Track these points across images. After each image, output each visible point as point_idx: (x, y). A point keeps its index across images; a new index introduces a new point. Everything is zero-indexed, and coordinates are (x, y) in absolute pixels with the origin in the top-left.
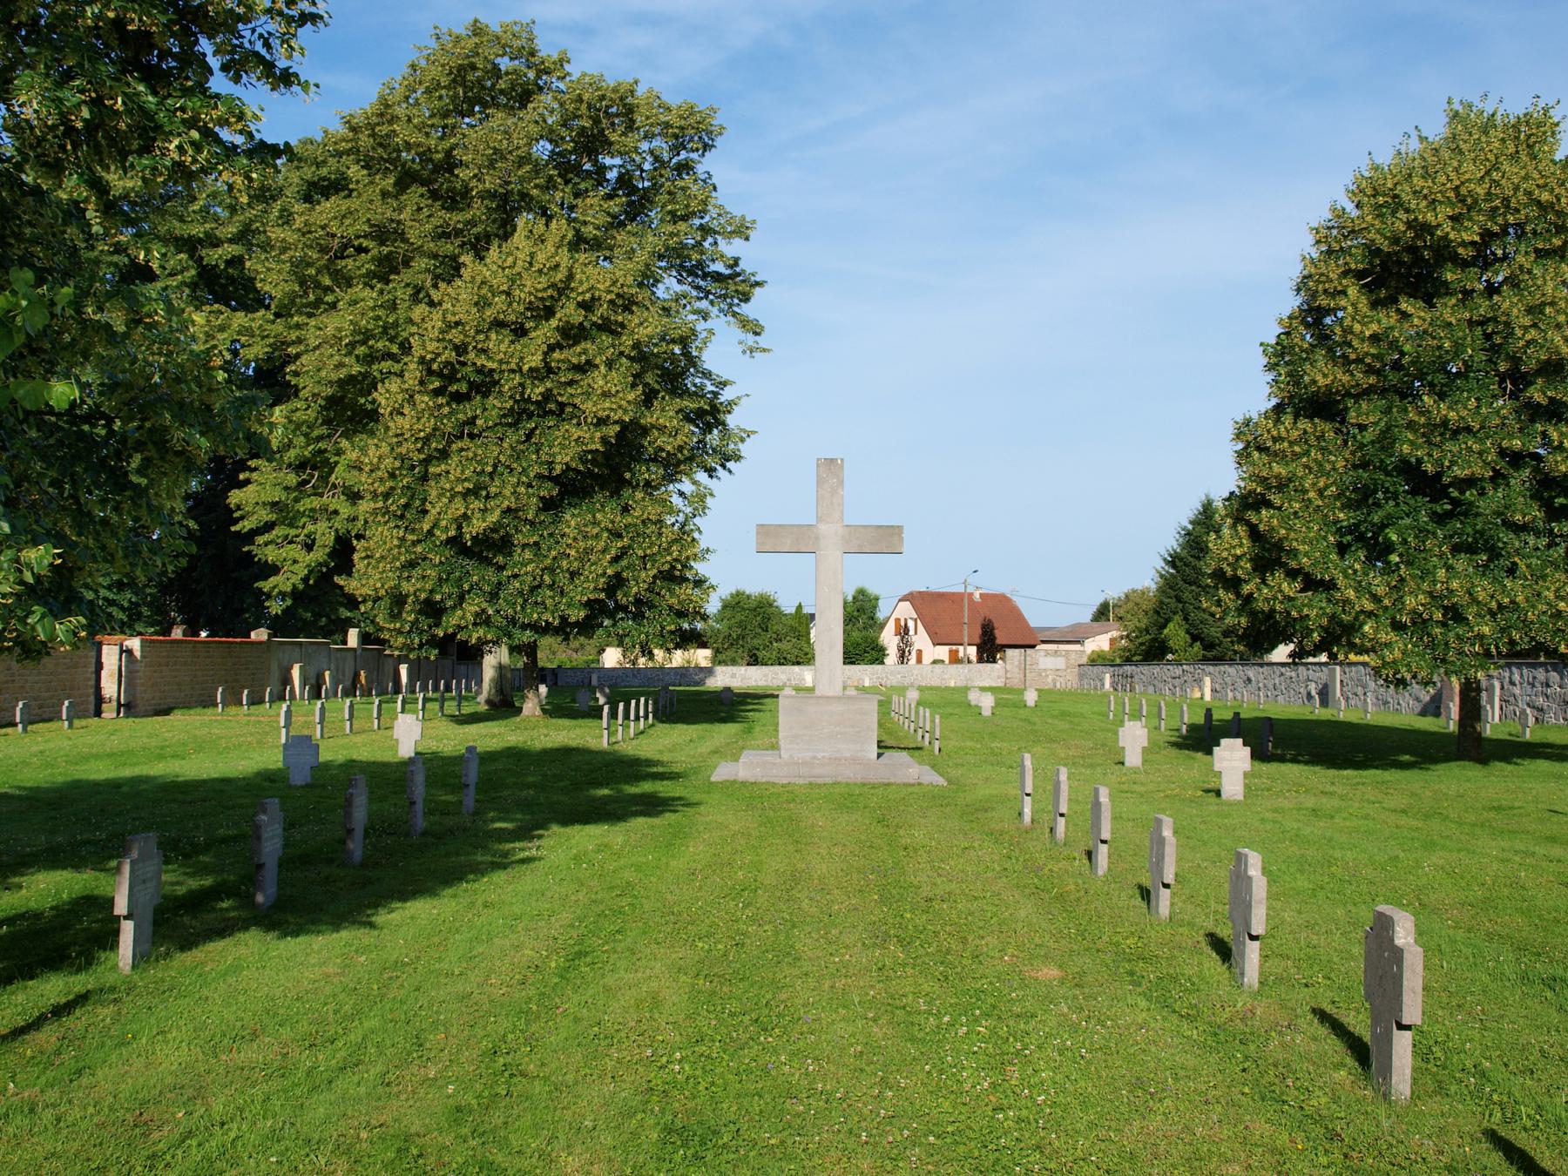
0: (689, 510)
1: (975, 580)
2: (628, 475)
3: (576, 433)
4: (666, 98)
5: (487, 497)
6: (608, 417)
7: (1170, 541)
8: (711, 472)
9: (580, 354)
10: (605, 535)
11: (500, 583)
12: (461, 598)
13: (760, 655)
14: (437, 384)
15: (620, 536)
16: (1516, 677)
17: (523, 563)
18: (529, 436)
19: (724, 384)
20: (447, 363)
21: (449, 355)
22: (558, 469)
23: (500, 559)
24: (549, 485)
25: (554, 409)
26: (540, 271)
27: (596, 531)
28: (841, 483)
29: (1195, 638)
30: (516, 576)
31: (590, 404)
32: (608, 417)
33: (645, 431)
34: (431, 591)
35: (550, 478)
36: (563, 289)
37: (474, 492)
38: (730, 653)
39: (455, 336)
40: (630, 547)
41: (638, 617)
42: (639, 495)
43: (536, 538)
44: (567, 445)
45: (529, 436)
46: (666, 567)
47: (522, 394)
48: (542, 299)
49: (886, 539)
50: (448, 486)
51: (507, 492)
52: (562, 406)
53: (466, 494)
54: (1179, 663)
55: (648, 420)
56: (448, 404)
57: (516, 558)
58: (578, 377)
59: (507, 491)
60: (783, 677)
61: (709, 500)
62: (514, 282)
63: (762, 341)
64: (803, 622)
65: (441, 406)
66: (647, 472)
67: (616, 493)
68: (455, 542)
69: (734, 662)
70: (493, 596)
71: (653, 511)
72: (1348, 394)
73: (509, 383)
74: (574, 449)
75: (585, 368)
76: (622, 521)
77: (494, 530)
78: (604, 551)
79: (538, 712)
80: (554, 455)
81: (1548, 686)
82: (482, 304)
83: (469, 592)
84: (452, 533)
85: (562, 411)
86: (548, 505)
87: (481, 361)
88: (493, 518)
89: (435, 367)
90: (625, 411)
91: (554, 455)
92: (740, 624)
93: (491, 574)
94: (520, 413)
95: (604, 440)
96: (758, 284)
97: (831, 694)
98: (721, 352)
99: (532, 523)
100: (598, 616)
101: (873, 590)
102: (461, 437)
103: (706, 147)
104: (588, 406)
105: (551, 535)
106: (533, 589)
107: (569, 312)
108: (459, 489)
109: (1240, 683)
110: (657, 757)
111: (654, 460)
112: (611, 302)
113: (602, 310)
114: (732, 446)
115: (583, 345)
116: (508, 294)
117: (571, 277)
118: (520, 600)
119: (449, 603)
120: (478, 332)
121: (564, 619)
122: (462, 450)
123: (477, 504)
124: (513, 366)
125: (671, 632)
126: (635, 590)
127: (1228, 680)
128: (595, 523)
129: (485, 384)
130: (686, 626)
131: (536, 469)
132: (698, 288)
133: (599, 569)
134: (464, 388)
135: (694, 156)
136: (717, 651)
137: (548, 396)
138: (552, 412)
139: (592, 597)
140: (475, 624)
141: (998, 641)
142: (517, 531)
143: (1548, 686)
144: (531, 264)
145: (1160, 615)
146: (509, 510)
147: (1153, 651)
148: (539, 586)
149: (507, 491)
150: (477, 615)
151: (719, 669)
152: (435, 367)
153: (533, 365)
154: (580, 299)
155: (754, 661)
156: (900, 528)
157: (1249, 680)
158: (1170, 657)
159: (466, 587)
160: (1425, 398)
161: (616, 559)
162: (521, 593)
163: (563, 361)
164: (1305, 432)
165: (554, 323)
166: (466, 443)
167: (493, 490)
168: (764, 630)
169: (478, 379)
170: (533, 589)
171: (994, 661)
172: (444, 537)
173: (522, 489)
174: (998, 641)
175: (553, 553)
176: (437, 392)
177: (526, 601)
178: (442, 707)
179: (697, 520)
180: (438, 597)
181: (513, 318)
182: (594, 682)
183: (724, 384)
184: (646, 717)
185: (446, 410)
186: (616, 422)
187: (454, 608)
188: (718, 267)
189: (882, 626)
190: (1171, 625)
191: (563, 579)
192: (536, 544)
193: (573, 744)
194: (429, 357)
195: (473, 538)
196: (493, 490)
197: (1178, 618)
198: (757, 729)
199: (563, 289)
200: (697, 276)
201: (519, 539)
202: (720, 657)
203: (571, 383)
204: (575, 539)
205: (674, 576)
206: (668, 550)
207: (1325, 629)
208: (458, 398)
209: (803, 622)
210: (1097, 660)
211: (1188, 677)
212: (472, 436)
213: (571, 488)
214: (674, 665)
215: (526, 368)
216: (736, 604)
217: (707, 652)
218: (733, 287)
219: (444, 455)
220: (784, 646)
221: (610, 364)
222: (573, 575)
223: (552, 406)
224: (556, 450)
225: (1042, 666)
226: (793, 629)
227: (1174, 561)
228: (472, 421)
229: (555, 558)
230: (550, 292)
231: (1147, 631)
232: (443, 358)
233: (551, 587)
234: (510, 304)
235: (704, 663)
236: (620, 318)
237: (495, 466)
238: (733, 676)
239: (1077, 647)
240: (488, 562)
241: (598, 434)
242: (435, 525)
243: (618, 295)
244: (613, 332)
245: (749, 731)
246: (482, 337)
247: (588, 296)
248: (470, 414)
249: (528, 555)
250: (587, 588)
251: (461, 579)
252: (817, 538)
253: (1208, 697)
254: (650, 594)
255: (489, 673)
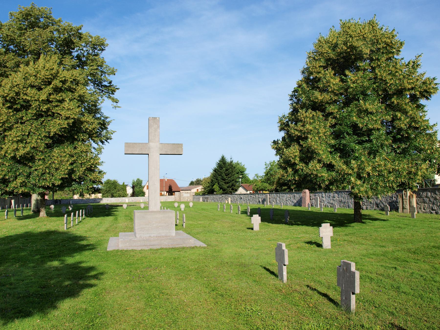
0: (96, 153)
1: (166, 176)
2: (76, 137)
3: (58, 122)
4: (91, 34)
5: (26, 143)
6: (69, 117)
7: (214, 166)
8: (102, 142)
9: (60, 97)
10: (68, 155)
11: (30, 172)
12: (16, 178)
13: (114, 195)
14: (9, 105)
15: (73, 156)
16: (324, 195)
17: (39, 166)
18: (42, 123)
19: (107, 118)
20: (12, 98)
21: (12, 94)
22: (52, 134)
23: (30, 164)
24: (49, 139)
25: (49, 114)
26: (47, 70)
27: (65, 154)
28: (159, 127)
29: (221, 188)
30: (36, 170)
31: (63, 112)
32: (69, 117)
33: (82, 123)
34: (5, 175)
35: (49, 137)
36: (55, 76)
37: (21, 141)
38: (106, 195)
39: (16, 89)
40: (76, 160)
41: (80, 183)
42: (80, 143)
43: (43, 157)
44: (55, 126)
45: (42, 123)
46: (89, 166)
47: (39, 108)
48: (47, 78)
49: (175, 150)
50: (11, 139)
51: (33, 141)
52: (53, 113)
53: (18, 142)
54: (217, 194)
55: (83, 119)
56: (13, 112)
57: (36, 164)
58: (59, 104)
59: (33, 141)
60: (121, 200)
61: (102, 150)
62: (38, 73)
63: (119, 104)
64: (124, 187)
65: (10, 112)
66: (81, 136)
67: (72, 143)
68: (14, 158)
69: (107, 197)
70: (28, 177)
71: (84, 148)
72: (327, 103)
73: (34, 105)
74: (58, 127)
75: (62, 101)
76: (74, 152)
77: (28, 154)
78: (68, 161)
79: (45, 215)
80: (50, 129)
81: (334, 197)
82: (26, 79)
83: (19, 175)
84: (12, 155)
85: (54, 115)
86: (48, 146)
87: (25, 97)
88: (28, 149)
89: (8, 98)
90: (76, 115)
91: (50, 129)
92: (109, 187)
93: (27, 169)
94: (39, 115)
95: (68, 124)
96: (117, 89)
97: (155, 210)
98: (106, 106)
99: (42, 152)
100: (67, 182)
101: (141, 179)
102: (18, 123)
103: (102, 50)
104: (63, 113)
105: (49, 156)
106: (43, 174)
107: (56, 83)
108: (15, 139)
109: (239, 199)
110: (84, 234)
111: (85, 132)
112: (71, 82)
113: (68, 84)
114: (109, 135)
115: (61, 93)
116: (36, 76)
117: (58, 72)
118: (38, 178)
119: (11, 179)
120: (24, 87)
121: (53, 184)
122: (17, 127)
123: (21, 145)
124: (36, 98)
125: (91, 188)
126: (78, 174)
127: (235, 198)
128: (65, 152)
129: (27, 106)
130: (95, 186)
131: (44, 134)
132: (100, 89)
133: (66, 167)
134: (19, 106)
135: (99, 52)
136: (103, 194)
137: (48, 109)
138: (50, 115)
139: (63, 176)
140: (21, 186)
141: (173, 190)
142: (37, 155)
143: (334, 197)
144: (44, 68)
145: (212, 183)
146: (34, 147)
147: (211, 192)
148: (45, 173)
149: (33, 141)
150: (21, 183)
151: (104, 199)
152: (8, 98)
153: (43, 98)
154: (61, 79)
155: (113, 196)
156: (182, 144)
157: (241, 198)
158: (215, 193)
159: (18, 174)
160: (361, 101)
161: (72, 164)
162: (38, 176)
163: (54, 98)
164: (313, 115)
165: (51, 86)
166: (19, 125)
167: (28, 141)
168: (114, 189)
169: (25, 104)
170: (43, 174)
171: (172, 195)
172: (9, 156)
173: (39, 141)
174: (173, 190)
175: (50, 162)
176: (9, 108)
177: (40, 179)
178: (15, 214)
179: (99, 156)
180: (7, 177)
181: (37, 84)
182: (71, 203)
183: (107, 118)
184: (82, 216)
185: (12, 114)
186: (72, 119)
187: (13, 181)
188: (106, 83)
189: (144, 187)
190: (215, 185)
191: (53, 171)
192: (43, 159)
193: (53, 229)
194: (5, 95)
195: (20, 157)
196: (28, 141)
197: (217, 184)
198: (119, 218)
199: (55, 76)
200: (99, 86)
201: (37, 157)
202: (104, 195)
203: (57, 106)
204: (57, 157)
205: (91, 170)
206: (89, 161)
207: (330, 180)
208: (17, 110)
209: (124, 187)
210: (197, 194)
211: (224, 198)
212: (22, 123)
213: (57, 140)
214: (92, 198)
215: (41, 99)
216: (108, 182)
217: (101, 194)
218: (110, 90)
219: (10, 128)
220: (120, 192)
221: (71, 100)
222: (57, 169)
223: (50, 113)
224: (51, 128)
225: (184, 196)
226: (122, 188)
227: (215, 170)
228: (21, 118)
229: (50, 164)
230: (50, 76)
231: (209, 187)
232: (10, 96)
233: (49, 173)
234: (36, 80)
235: (100, 197)
236: (74, 87)
237: (29, 133)
238: (108, 200)
239: (190, 191)
240: (26, 165)
241: (66, 122)
242: (6, 152)
243: (74, 79)
244: (72, 92)
245: (116, 219)
246: (25, 89)
247: (63, 79)
248: (21, 115)
249: (41, 162)
250: (62, 173)
251: (16, 171)
252: (149, 148)
253: (230, 203)
254: (84, 174)
255: (33, 202)
